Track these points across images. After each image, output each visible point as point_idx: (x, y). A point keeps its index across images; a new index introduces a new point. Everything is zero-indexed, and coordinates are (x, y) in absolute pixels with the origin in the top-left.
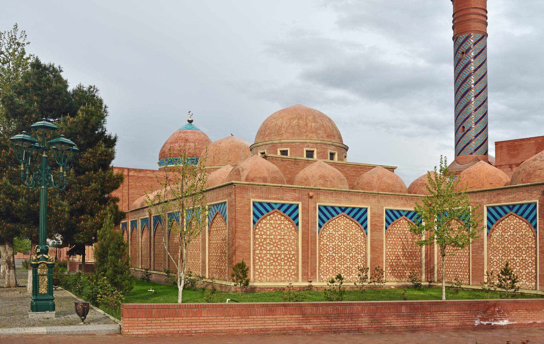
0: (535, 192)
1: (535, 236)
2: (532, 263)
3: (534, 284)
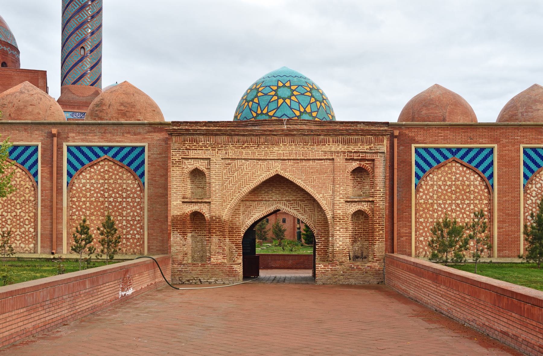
0: (37, 132)
1: (35, 189)
2: (30, 221)
3: (32, 245)
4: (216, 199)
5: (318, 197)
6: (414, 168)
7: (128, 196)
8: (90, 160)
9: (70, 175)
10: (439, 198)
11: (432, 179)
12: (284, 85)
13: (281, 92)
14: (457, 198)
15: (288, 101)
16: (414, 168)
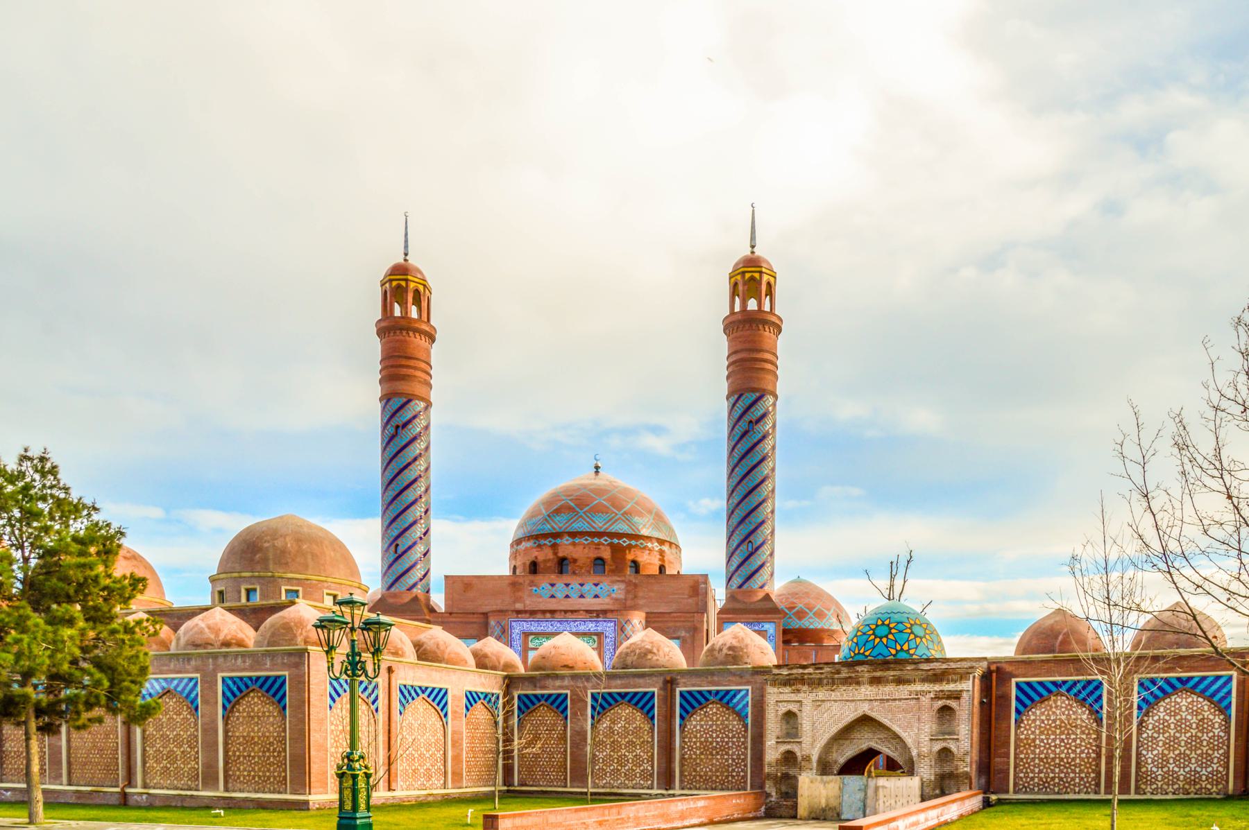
1: (652, 729)
4: (806, 739)
5: (903, 735)
6: (1014, 703)
7: (734, 736)
8: (700, 703)
9: (682, 717)
10: (1042, 733)
11: (1034, 714)
12: (883, 624)
13: (878, 632)
14: (1062, 733)
15: (884, 640)
16: (1014, 703)
